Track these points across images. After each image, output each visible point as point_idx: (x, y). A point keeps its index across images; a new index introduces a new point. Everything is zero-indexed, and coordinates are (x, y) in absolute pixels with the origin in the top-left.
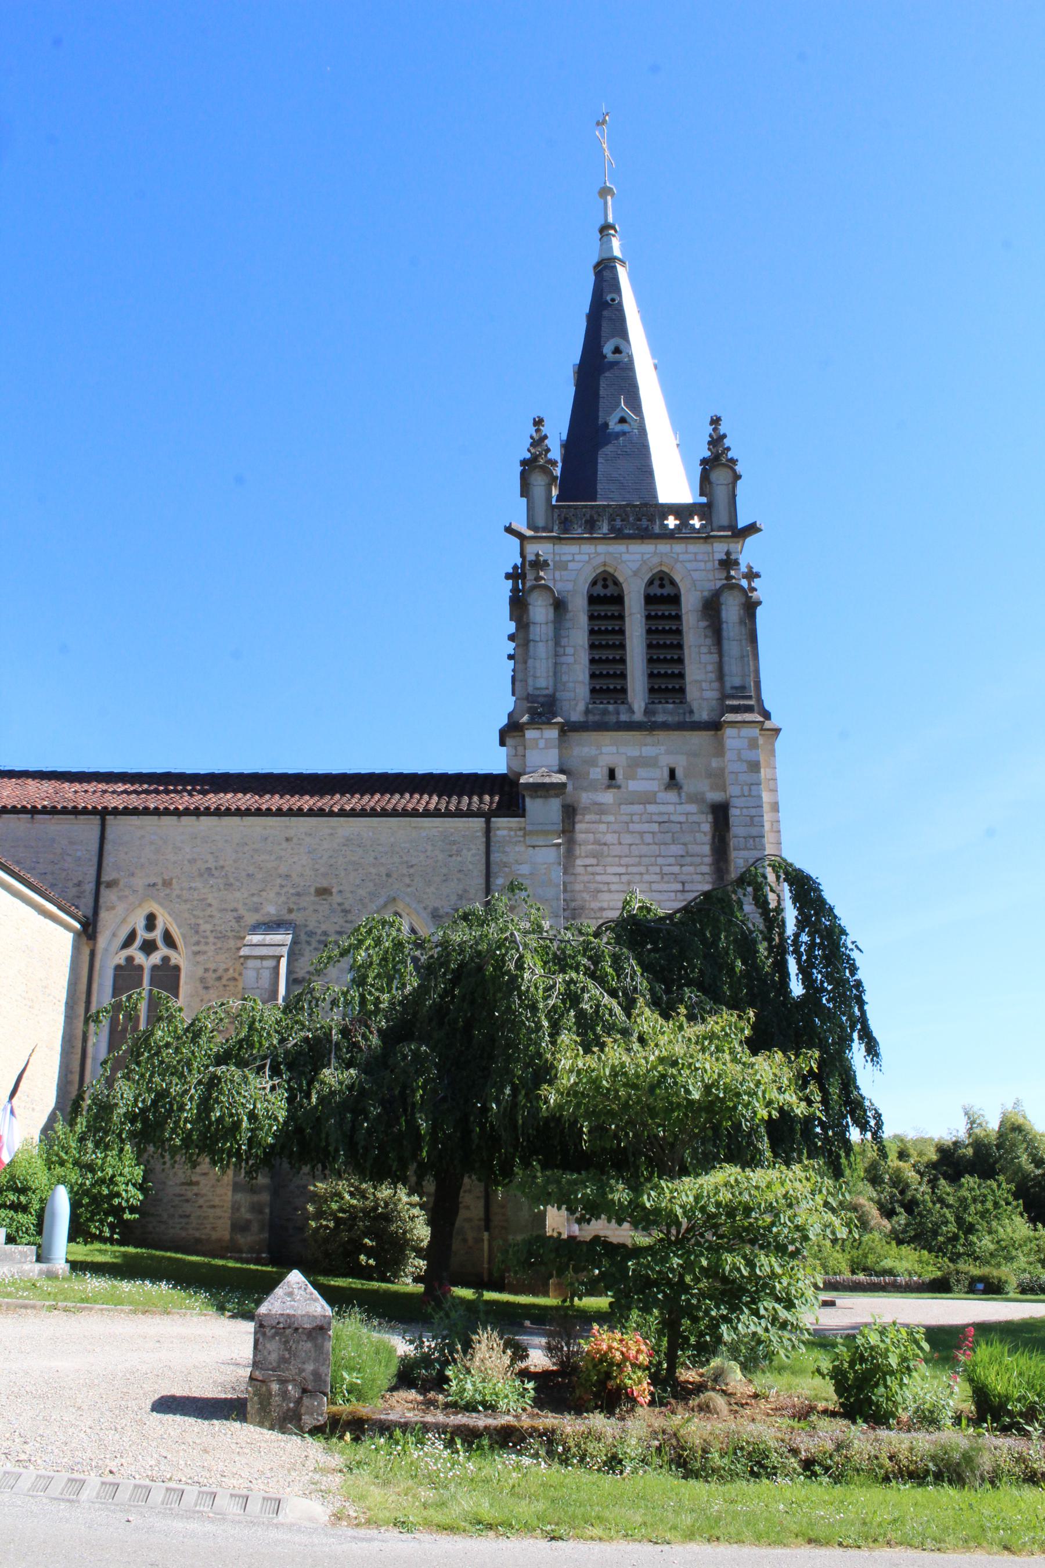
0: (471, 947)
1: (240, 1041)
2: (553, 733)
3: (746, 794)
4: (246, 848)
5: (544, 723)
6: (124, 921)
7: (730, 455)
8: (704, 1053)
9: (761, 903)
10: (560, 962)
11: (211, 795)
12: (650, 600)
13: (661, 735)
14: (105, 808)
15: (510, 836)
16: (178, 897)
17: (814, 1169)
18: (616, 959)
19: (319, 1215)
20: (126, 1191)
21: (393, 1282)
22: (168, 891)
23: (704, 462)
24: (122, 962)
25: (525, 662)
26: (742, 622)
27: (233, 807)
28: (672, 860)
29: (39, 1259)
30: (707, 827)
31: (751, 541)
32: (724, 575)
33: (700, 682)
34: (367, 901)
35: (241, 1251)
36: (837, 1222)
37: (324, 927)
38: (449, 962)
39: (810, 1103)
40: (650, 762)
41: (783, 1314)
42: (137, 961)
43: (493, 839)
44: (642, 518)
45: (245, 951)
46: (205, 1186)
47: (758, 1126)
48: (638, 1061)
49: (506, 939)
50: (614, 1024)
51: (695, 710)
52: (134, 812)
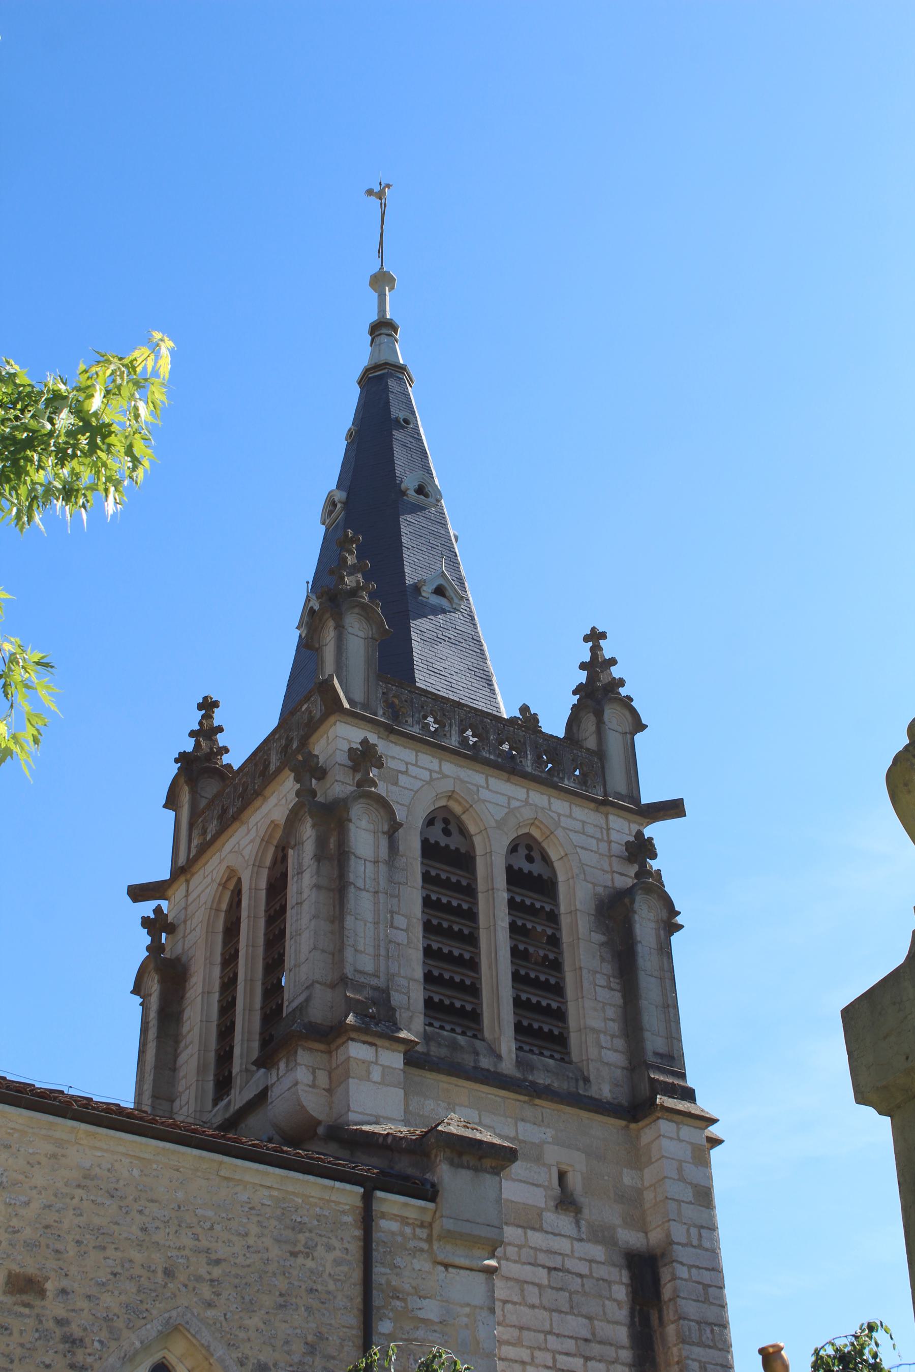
3: (695, 1243)
5: (381, 1036)
13: (547, 1108)
15: (402, 1234)
28: (570, 1345)
30: (621, 1292)
32: (633, 869)
33: (597, 1031)
34: (120, 1324)
51: (592, 1078)
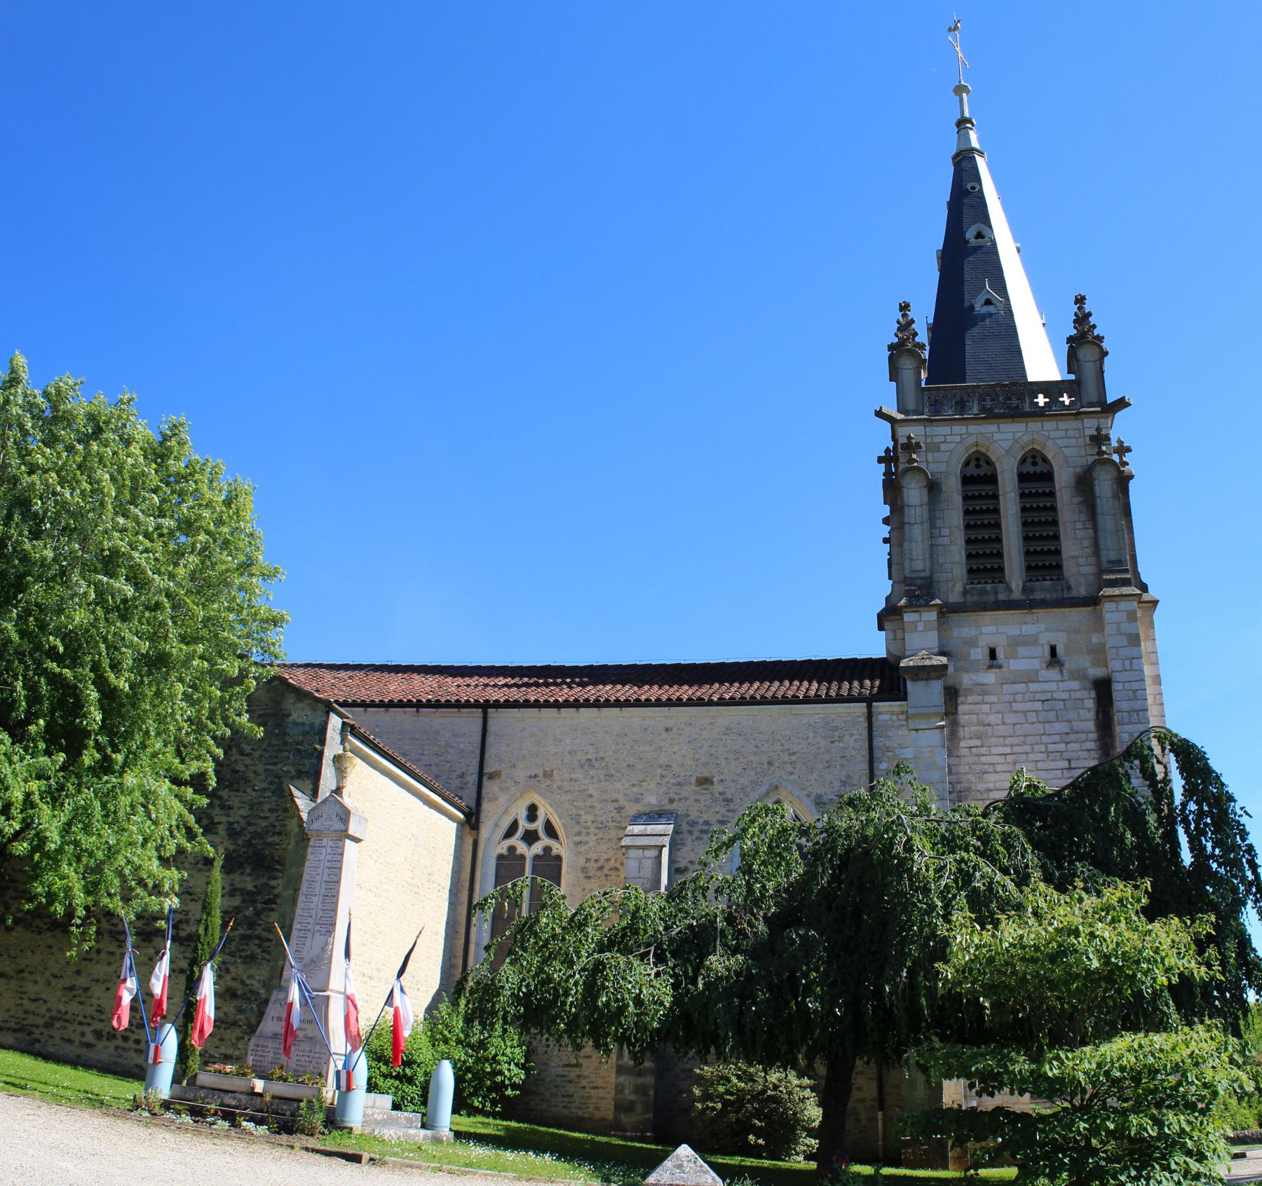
0: (857, 832)
1: (624, 929)
2: (932, 616)
4: (626, 739)
6: (506, 811)
7: (1096, 332)
8: (1101, 922)
9: (1149, 775)
10: (949, 843)
11: (590, 687)
12: (1023, 478)
13: (1041, 613)
14: (487, 701)
16: (559, 788)
17: (1217, 1027)
18: (1007, 840)
19: (706, 1097)
20: (509, 1070)
21: (783, 1160)
22: (549, 782)
23: (1070, 340)
24: (504, 852)
25: (901, 546)
26: (1115, 497)
27: (612, 699)
28: (1057, 738)
29: (423, 1126)
31: (1120, 416)
33: (1076, 557)
35: (625, 1130)
36: (1244, 1077)
37: (705, 817)
38: (836, 847)
39: (1209, 966)
40: (1032, 641)
41: (1195, 1166)
42: (519, 851)
43: (875, 724)
44: (1014, 397)
45: (626, 841)
46: (588, 1067)
47: (1162, 991)
48: (1035, 933)
49: (893, 822)
50: (1009, 900)
52: (515, 705)
